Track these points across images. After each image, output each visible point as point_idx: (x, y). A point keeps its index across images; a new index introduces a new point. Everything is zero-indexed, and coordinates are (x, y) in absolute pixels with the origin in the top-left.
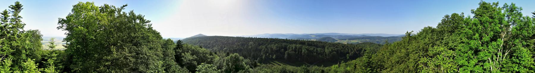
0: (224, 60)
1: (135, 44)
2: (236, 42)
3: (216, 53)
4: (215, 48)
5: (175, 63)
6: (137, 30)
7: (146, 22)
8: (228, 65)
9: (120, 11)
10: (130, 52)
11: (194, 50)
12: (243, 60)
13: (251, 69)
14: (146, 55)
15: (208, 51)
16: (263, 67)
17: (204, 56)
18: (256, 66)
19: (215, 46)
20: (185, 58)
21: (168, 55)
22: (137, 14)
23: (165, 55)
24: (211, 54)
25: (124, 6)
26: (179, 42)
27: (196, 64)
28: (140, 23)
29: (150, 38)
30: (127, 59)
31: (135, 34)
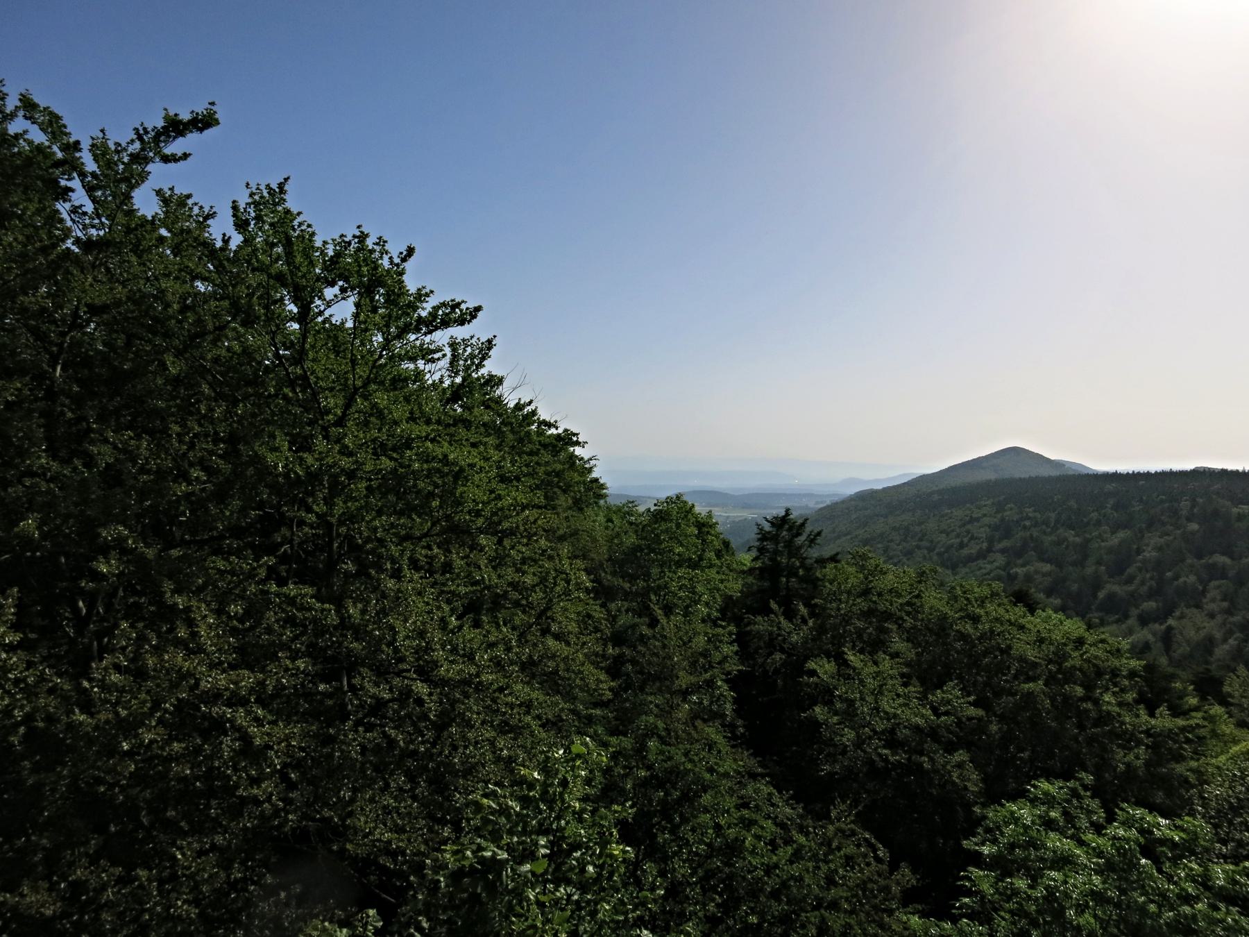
1: (314, 566)
3: (1209, 687)
5: (732, 761)
6: (332, 402)
7: (434, 322)
9: (134, 178)
10: (250, 656)
11: (941, 628)
14: (426, 672)
17: (1065, 706)
19: (1195, 599)
20: (849, 714)
21: (662, 677)
22: (327, 227)
23: (633, 672)
24: (1154, 693)
25: (175, 127)
26: (784, 535)
27: (973, 781)
28: (362, 328)
29: (474, 492)
30: (218, 726)
31: (302, 444)
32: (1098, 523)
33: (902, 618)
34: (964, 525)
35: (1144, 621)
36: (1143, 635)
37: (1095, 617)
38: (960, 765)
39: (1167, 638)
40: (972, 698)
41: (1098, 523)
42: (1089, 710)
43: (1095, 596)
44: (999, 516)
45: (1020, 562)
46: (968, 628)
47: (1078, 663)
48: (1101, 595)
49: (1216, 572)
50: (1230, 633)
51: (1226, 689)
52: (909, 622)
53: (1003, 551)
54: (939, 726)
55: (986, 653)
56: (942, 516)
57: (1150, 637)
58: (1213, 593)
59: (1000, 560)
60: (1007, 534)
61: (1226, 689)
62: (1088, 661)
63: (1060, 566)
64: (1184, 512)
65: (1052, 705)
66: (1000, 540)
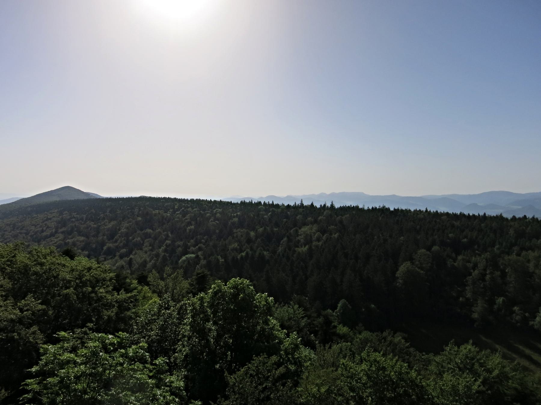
0: (182, 313)
2: (241, 225)
4: (139, 257)
8: (200, 331)
11: (25, 270)
12: (269, 311)
13: (305, 352)
15: (107, 268)
16: (365, 342)
17: (84, 298)
18: (328, 337)
19: (139, 246)
24: (120, 285)
32: (104, 219)
33: (5, 268)
34: (43, 222)
35: (121, 257)
36: (121, 262)
37: (101, 258)
38: (34, 333)
39: (130, 263)
40: (40, 301)
41: (104, 219)
42: (93, 297)
43: (103, 249)
44: (61, 217)
45: (70, 237)
46: (38, 268)
47: (88, 278)
48: (105, 248)
49: (147, 236)
50: (152, 258)
51: (149, 279)
52: (9, 269)
53: (62, 233)
54: (23, 317)
55: (48, 279)
56: (33, 218)
57: (124, 263)
58: (146, 244)
59: (61, 236)
60: (64, 225)
61: (149, 279)
62: (93, 276)
63: (87, 237)
64: (136, 213)
65: (77, 297)
66: (61, 228)
